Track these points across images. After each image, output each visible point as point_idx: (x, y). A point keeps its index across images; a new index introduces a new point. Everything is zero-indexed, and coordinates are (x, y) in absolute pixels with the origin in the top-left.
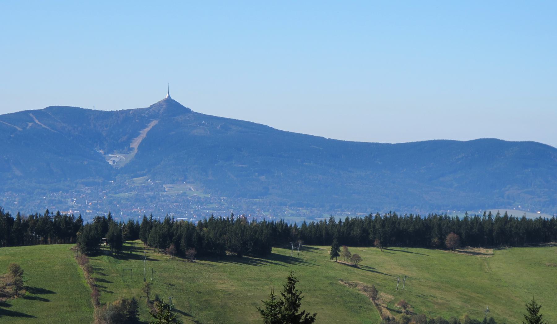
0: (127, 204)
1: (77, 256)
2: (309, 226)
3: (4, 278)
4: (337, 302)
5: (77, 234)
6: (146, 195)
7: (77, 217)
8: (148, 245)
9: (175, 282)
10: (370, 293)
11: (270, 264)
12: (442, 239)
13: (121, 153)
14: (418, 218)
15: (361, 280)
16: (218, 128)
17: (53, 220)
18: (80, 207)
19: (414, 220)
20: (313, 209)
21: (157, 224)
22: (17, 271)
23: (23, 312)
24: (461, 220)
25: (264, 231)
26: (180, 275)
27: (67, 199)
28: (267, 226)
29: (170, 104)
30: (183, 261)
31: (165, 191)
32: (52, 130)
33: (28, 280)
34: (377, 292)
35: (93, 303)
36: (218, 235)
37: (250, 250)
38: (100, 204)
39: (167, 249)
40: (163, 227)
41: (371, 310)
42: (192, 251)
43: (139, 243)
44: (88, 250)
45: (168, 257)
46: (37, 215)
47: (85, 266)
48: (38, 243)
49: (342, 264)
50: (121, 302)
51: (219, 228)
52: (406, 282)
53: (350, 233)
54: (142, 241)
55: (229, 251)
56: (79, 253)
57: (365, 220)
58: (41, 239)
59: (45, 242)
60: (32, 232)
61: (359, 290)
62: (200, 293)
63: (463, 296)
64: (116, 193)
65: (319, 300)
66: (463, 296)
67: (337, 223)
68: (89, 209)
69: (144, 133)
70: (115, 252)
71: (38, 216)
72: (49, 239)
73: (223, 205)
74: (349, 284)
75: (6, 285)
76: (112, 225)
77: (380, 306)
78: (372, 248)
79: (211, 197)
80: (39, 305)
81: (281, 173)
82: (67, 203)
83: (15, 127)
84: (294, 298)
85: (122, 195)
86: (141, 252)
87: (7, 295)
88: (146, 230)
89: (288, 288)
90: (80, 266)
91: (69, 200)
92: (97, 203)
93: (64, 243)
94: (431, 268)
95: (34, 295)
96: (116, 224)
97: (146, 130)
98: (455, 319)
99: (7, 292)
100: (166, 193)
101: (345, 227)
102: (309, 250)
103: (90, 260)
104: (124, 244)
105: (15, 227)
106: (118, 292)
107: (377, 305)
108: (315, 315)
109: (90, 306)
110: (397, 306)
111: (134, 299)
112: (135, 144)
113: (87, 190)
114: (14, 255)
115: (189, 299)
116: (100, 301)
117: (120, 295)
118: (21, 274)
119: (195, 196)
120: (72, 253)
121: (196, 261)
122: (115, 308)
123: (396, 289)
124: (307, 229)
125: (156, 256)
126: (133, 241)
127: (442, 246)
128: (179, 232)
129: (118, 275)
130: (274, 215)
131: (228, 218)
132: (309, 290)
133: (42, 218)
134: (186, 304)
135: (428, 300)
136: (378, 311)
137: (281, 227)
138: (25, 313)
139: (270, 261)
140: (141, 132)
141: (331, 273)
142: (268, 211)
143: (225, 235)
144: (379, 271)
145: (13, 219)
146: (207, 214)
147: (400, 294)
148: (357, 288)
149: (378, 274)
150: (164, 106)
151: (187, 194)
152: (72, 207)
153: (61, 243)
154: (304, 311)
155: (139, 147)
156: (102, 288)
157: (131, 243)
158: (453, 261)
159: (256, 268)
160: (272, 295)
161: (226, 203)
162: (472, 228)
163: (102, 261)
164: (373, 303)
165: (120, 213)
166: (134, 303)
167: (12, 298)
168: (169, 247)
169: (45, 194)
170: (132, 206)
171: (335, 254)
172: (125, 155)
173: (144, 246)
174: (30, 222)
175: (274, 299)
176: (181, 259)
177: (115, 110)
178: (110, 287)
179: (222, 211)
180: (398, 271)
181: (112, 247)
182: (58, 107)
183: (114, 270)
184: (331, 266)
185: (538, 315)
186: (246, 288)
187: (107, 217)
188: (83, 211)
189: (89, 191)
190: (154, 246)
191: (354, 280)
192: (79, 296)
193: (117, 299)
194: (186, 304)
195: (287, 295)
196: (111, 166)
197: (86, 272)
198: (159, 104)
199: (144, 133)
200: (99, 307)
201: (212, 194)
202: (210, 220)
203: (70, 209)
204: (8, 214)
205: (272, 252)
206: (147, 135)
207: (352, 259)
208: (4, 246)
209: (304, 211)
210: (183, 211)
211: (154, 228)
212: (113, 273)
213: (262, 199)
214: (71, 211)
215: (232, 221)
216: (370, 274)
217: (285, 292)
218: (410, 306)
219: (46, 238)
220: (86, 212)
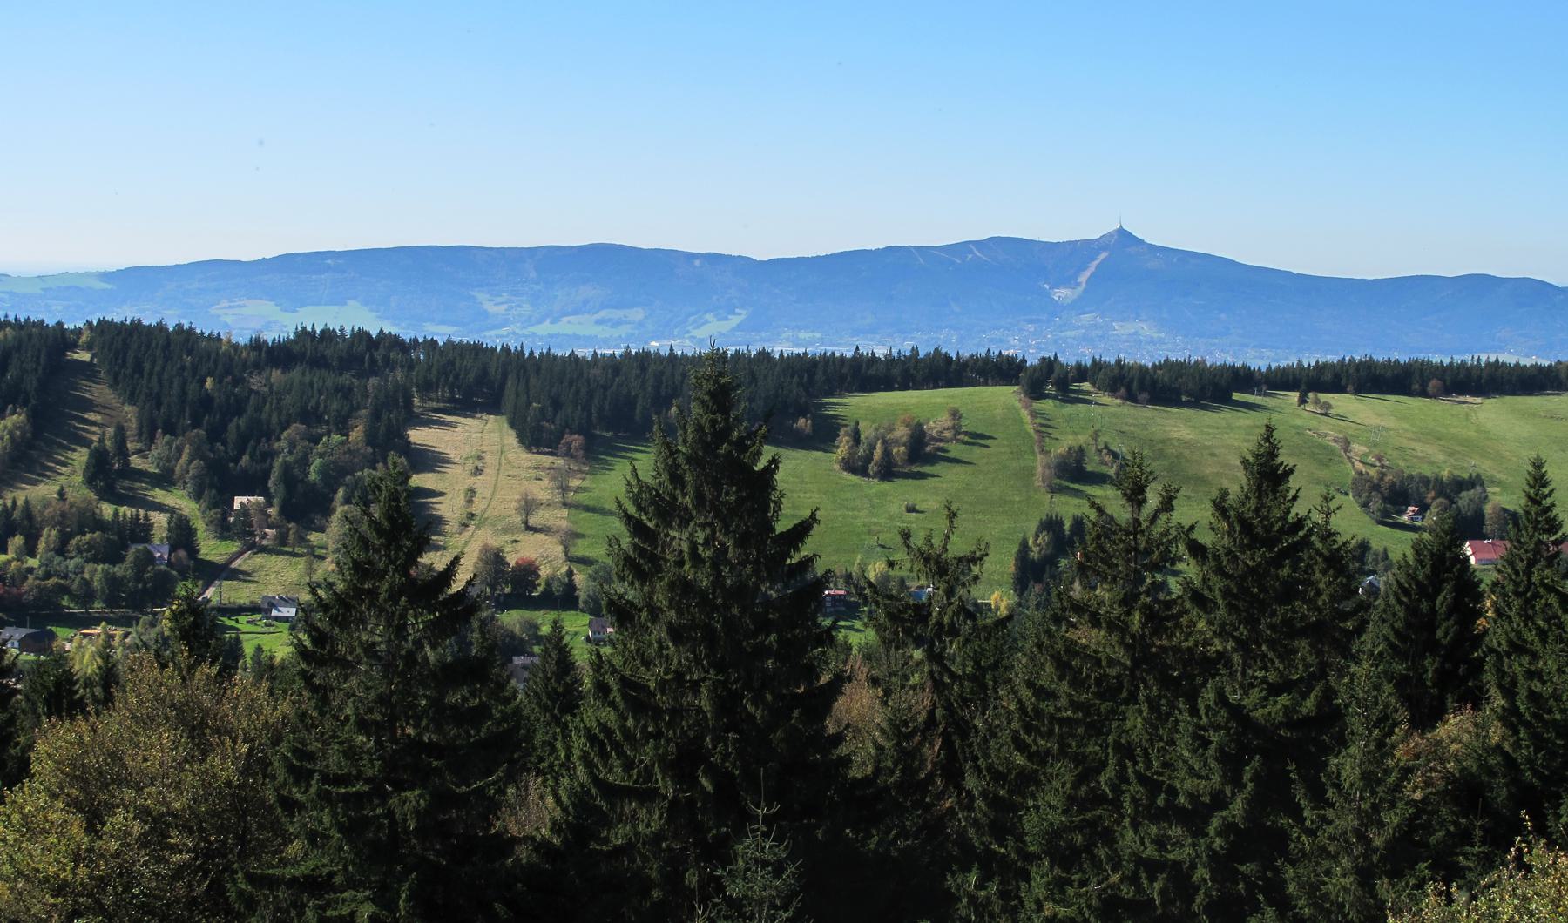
9: (1126, 428)
12: (1424, 384)
21: (1107, 365)
22: (955, 414)
28: (1228, 370)
29: (1121, 232)
33: (966, 425)
35: (1037, 450)
41: (1342, 463)
42: (1145, 396)
43: (1087, 385)
45: (1118, 401)
48: (979, 384)
59: (986, 384)
62: (1152, 441)
69: (1093, 266)
96: (1062, 365)
105: (953, 367)
107: (1349, 458)
108: (1295, 466)
109: (1033, 452)
110: (1371, 459)
112: (1083, 279)
114: (952, 397)
127: (1424, 394)
141: (1298, 422)
152: (1014, 346)
162: (1458, 374)
163: (1047, 405)
166: (1081, 450)
169: (984, 332)
171: (1303, 401)
173: (1092, 390)
178: (1055, 434)
180: (1375, 421)
181: (1057, 390)
185: (1544, 470)
186: (1204, 437)
198: (1110, 235)
199: (1093, 266)
209: (1269, 353)
216: (1342, 423)
219: (986, 380)
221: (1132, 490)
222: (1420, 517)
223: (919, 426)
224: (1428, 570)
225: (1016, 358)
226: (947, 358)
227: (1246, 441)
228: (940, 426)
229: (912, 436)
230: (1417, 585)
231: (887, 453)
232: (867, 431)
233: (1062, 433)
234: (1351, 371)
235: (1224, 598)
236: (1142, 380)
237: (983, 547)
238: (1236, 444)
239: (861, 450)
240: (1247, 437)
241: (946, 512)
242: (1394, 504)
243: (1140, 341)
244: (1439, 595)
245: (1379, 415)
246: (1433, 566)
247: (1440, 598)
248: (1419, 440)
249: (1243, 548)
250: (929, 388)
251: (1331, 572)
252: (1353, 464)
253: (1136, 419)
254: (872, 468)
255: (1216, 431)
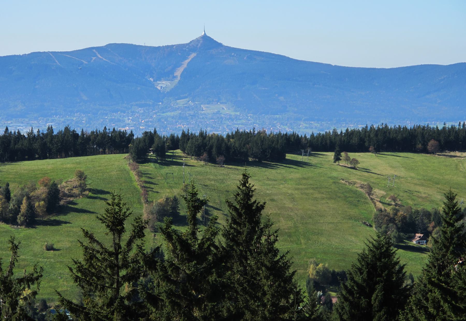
0: (173, 121)
1: (130, 164)
2: (316, 136)
3: (71, 182)
4: (339, 197)
5: (129, 145)
6: (188, 113)
7: (129, 132)
8: (186, 154)
9: (208, 183)
10: (366, 189)
11: (285, 168)
12: (425, 144)
13: (167, 80)
14: (405, 129)
15: (358, 179)
16: (245, 58)
17: (110, 135)
18: (135, 124)
19: (402, 130)
20: (323, 122)
21: (193, 137)
22: (81, 176)
23: (86, 209)
24: (440, 129)
25: (280, 141)
26: (212, 177)
27: (124, 118)
28: (282, 137)
29: (205, 38)
30: (215, 166)
31: (203, 110)
32: (111, 63)
33: (90, 184)
34: (372, 188)
35: (143, 200)
36: (242, 145)
37: (268, 156)
38: (151, 122)
39: (202, 157)
40: (198, 139)
41: (367, 203)
42: (221, 158)
43: (179, 152)
44: (138, 158)
45: (202, 163)
46: (97, 131)
47: (136, 171)
48: (98, 153)
49: (343, 167)
50: (165, 199)
51: (243, 139)
52: (395, 180)
53: (349, 142)
54: (182, 150)
55: (251, 157)
56: (131, 161)
57: (362, 130)
58: (101, 150)
59: (104, 153)
60: (93, 145)
61: (357, 187)
62: (228, 192)
63: (442, 191)
64: (164, 113)
65: (324, 196)
66: (442, 191)
67: (339, 133)
68: (142, 126)
69: (185, 63)
70: (160, 160)
71: (98, 132)
72: (107, 150)
73: (249, 120)
74: (349, 183)
75: (73, 188)
76: (157, 138)
77: (374, 200)
78: (368, 153)
79: (240, 114)
80: (99, 203)
81: (297, 94)
82: (125, 121)
83: (82, 60)
84: (248, 190)
85: (169, 114)
86: (180, 159)
87: (74, 195)
88: (184, 142)
89: (243, 182)
90: (132, 172)
91: (126, 119)
92: (149, 121)
93: (119, 153)
94: (416, 169)
95: (95, 196)
96: (160, 138)
97: (187, 61)
98: (435, 210)
99: (74, 193)
100: (203, 112)
101: (345, 136)
102: (316, 155)
103: (140, 167)
104: (167, 154)
105: (80, 140)
106: (162, 192)
107: (372, 199)
108: (265, 203)
109: (140, 203)
110: (388, 200)
111: (175, 197)
112: (178, 73)
113: (141, 110)
114: (79, 163)
115: (219, 196)
116: (148, 199)
117: (165, 194)
118: (85, 178)
119: (227, 114)
120: (125, 161)
121: (225, 166)
122: (160, 204)
123: (387, 186)
124: (315, 139)
125: (193, 163)
126: (174, 151)
127: (425, 151)
128: (211, 143)
129: (163, 178)
130: (291, 128)
131: (250, 131)
132: (317, 188)
133: (101, 133)
134: (217, 201)
135: (413, 194)
136: (373, 204)
137: (293, 137)
138: (89, 210)
139: (285, 165)
140: (183, 63)
141: (335, 174)
142: (286, 125)
143: (248, 144)
144: (373, 172)
145: (78, 134)
146: (235, 127)
147: (391, 190)
148: (355, 186)
149: (373, 175)
150: (201, 42)
151: (221, 112)
152: (129, 124)
153: (117, 153)
154: (256, 201)
155: (181, 75)
156: (149, 189)
157: (173, 153)
158: (434, 163)
159: (273, 171)
160: (193, 185)
161: (252, 119)
162: (449, 136)
163: (150, 167)
164: (369, 198)
165: (167, 129)
166: (175, 200)
167: (78, 198)
168: (203, 155)
169: (106, 114)
170: (176, 123)
171: (337, 159)
172: (170, 82)
173: (183, 155)
174: (92, 137)
175: (194, 189)
176: (213, 165)
177: (161, 46)
178: (156, 188)
179: (249, 125)
180: (389, 172)
181: (158, 155)
182: (115, 44)
183: (159, 174)
184: (334, 168)
185: (455, 202)
186: (265, 187)
187: (153, 132)
188: (138, 128)
189: (142, 111)
190: (191, 154)
191: (353, 179)
192: (132, 195)
193: (162, 198)
194: (217, 201)
195: (243, 188)
196: (159, 91)
197: (136, 177)
198: (197, 40)
199: (185, 63)
200: (147, 204)
201: (241, 112)
202: (236, 132)
203: (127, 126)
204: (74, 131)
205: (287, 158)
206: (187, 65)
207: (351, 162)
208: (71, 157)
209: (316, 124)
210: (218, 126)
211: (190, 140)
212: (158, 177)
213: (281, 115)
214: (128, 128)
215: (254, 133)
216: (366, 174)
217: (240, 186)
218: (398, 200)
219: (105, 150)
220: (140, 128)
221: (113, 223)
222: (425, 241)
223: (55, 185)
224: (365, 275)
225: (126, 133)
226: (75, 135)
227: (297, 189)
228: (70, 185)
229: (49, 194)
230: (357, 287)
231: (31, 207)
232: (15, 191)
233: (161, 188)
234: (372, 136)
235: (168, 298)
236: (219, 148)
237: (39, 270)
238: (290, 192)
239: (11, 205)
240: (297, 186)
241: (10, 245)
242: (406, 232)
243: (222, 118)
244: (373, 293)
245: (392, 167)
246: (368, 273)
247: (374, 296)
248: (422, 185)
249: (182, 261)
250: (61, 157)
251: (271, 278)
252: (375, 204)
253: (216, 175)
254: (20, 219)
255: (275, 183)
